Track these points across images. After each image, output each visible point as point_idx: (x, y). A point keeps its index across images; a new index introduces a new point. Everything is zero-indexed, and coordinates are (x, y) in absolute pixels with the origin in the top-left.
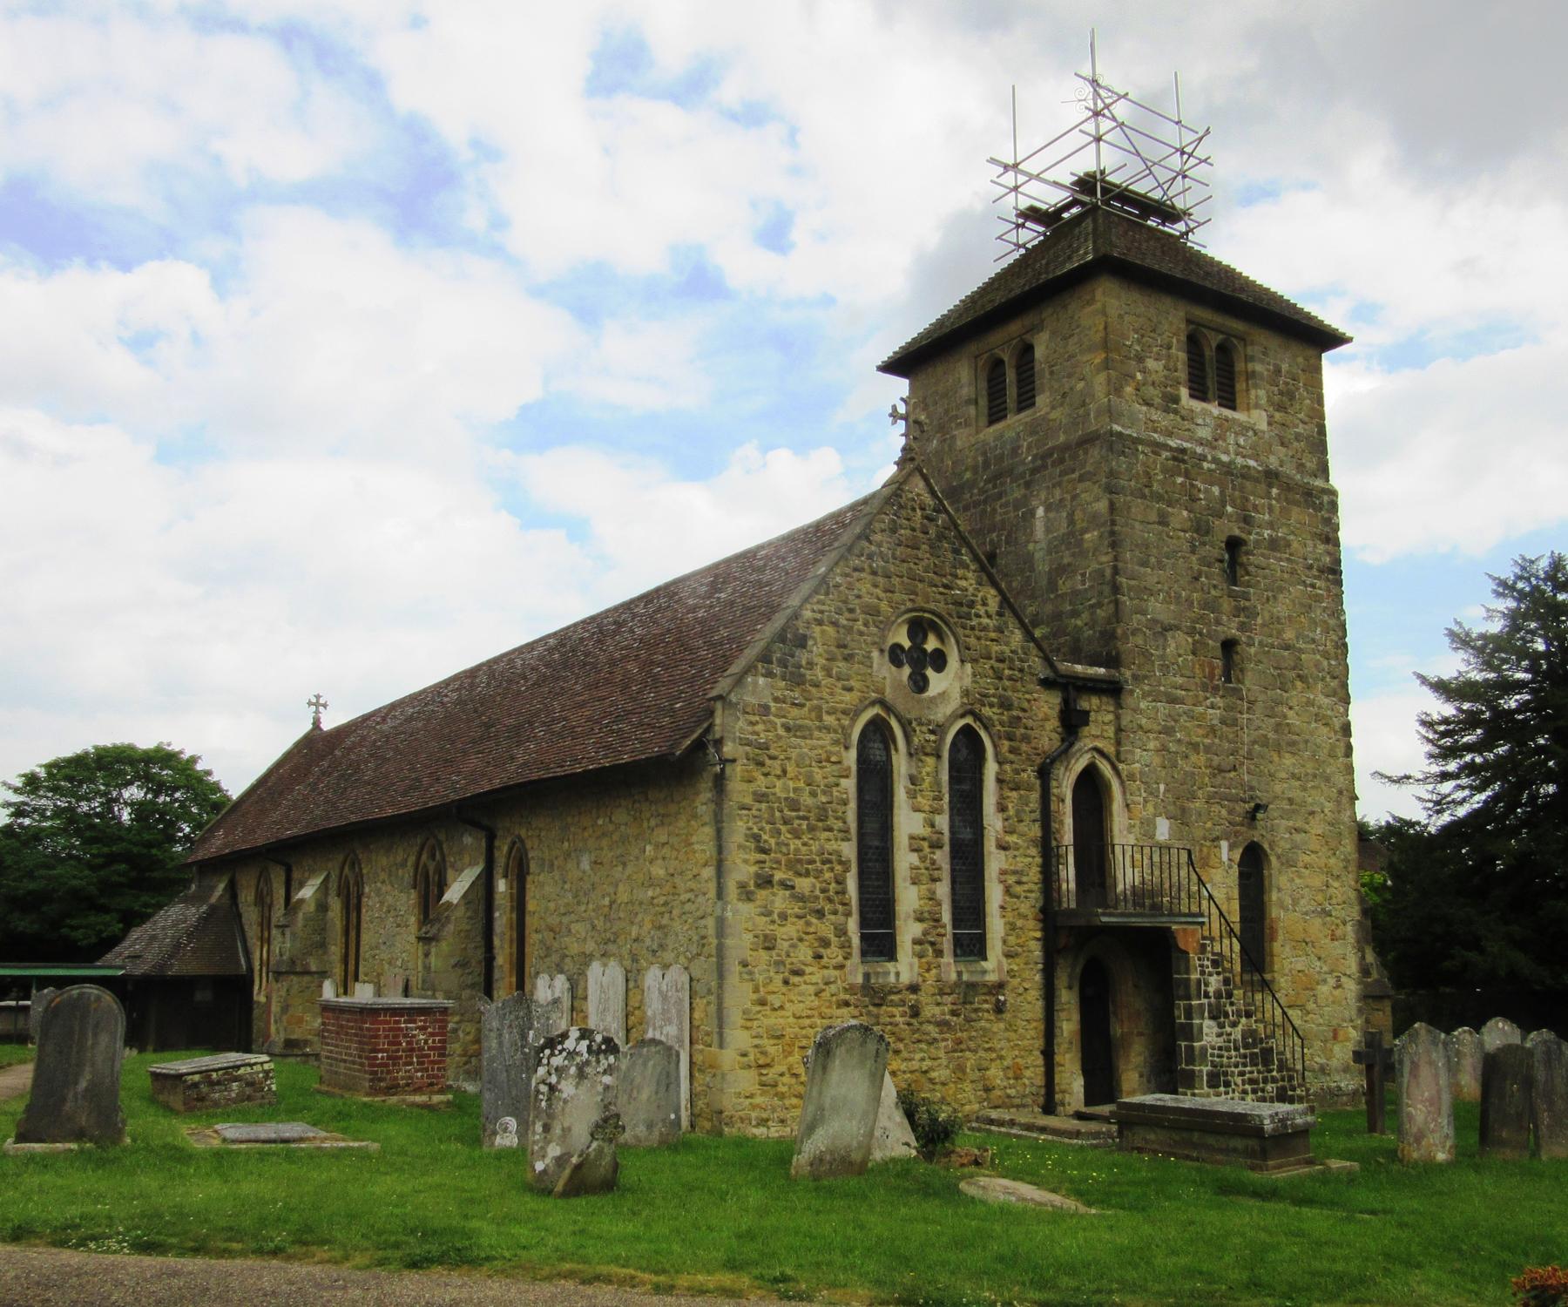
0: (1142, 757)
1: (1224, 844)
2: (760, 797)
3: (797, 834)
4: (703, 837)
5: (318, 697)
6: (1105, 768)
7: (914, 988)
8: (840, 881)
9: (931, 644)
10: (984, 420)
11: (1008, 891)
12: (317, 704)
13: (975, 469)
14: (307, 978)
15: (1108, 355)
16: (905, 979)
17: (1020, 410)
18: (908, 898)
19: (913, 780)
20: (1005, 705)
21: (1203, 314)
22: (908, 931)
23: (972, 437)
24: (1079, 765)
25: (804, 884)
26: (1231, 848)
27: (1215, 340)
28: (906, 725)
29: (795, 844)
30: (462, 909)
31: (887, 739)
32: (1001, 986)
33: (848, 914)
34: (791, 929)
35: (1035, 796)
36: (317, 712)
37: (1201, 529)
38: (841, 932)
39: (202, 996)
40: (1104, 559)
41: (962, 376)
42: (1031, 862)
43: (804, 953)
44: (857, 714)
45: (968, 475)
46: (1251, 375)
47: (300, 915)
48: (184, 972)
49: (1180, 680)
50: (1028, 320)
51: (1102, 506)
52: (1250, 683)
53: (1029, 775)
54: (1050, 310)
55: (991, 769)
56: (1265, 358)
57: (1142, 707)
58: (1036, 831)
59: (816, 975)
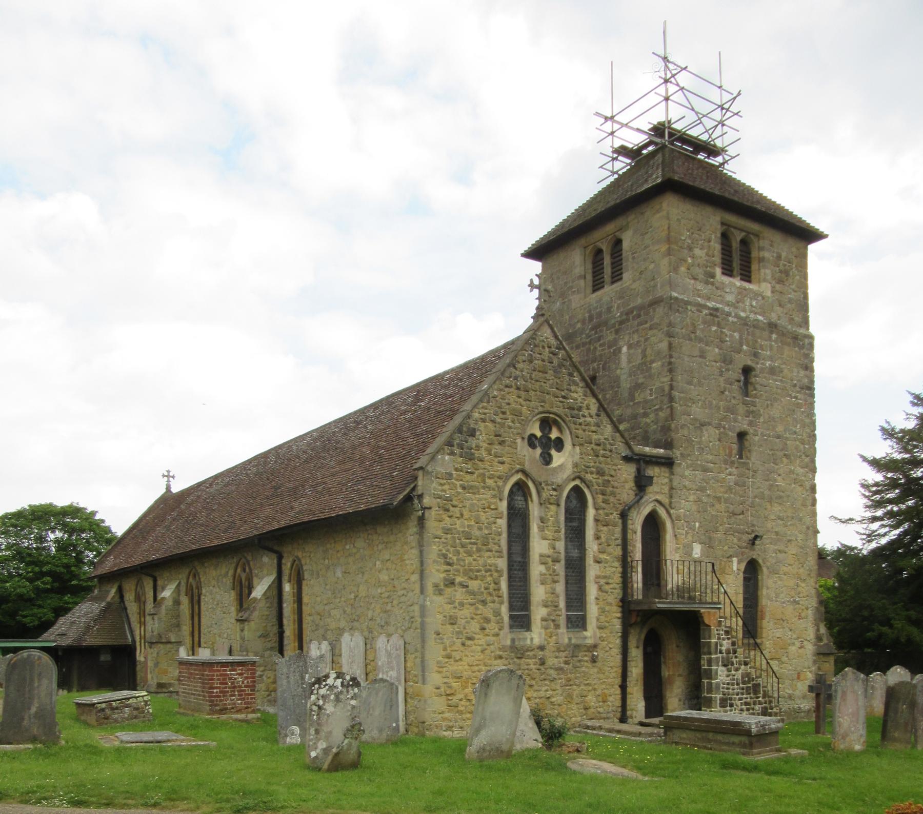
0: (685, 505)
1: (735, 560)
2: (447, 531)
3: (470, 554)
4: (412, 554)
5: (168, 472)
6: (662, 512)
7: (542, 648)
8: (497, 583)
9: (554, 434)
10: (589, 289)
11: (600, 589)
12: (168, 476)
13: (583, 322)
14: (169, 646)
15: (672, 239)
16: (537, 641)
17: (613, 283)
18: (538, 593)
19: (542, 520)
20: (601, 473)
21: (732, 219)
22: (538, 613)
23: (583, 300)
24: (646, 511)
25: (474, 585)
26: (739, 562)
27: (738, 236)
28: (538, 485)
29: (469, 559)
30: (264, 602)
31: (526, 494)
32: (595, 646)
33: (501, 603)
34: (467, 612)
35: (618, 530)
36: (168, 481)
37: (727, 360)
38: (497, 613)
39: (105, 658)
40: (665, 379)
41: (576, 259)
42: (615, 570)
43: (474, 627)
44: (507, 478)
45: (579, 325)
46: (761, 260)
47: (163, 607)
48: (93, 644)
49: (710, 457)
50: (620, 222)
51: (664, 346)
52: (755, 459)
53: (615, 517)
54: (633, 216)
55: (591, 513)
56: (770, 246)
57: (686, 473)
58: (618, 551)
59: (481, 640)
